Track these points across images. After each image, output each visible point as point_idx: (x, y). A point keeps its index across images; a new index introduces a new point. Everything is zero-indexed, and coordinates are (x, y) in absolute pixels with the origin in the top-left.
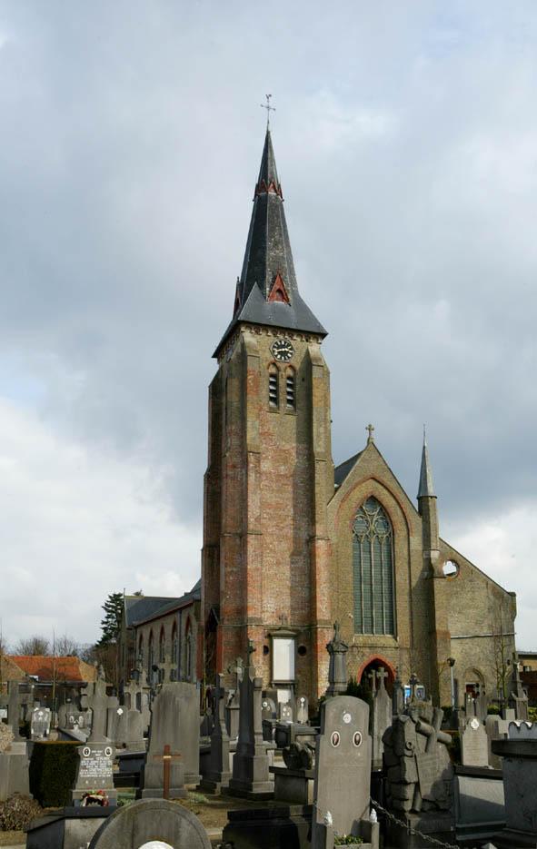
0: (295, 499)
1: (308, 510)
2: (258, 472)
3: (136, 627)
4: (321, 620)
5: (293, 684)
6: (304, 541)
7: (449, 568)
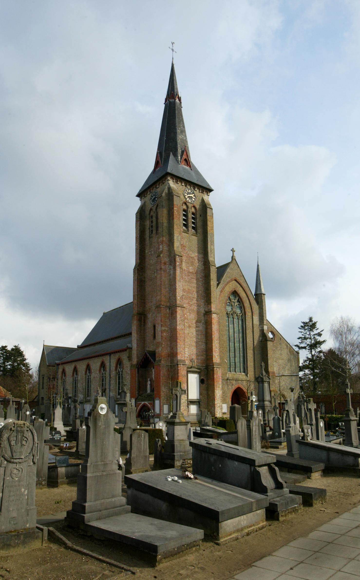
0: (197, 288)
1: (206, 296)
2: (181, 268)
3: (58, 365)
5: (199, 402)
6: (202, 314)
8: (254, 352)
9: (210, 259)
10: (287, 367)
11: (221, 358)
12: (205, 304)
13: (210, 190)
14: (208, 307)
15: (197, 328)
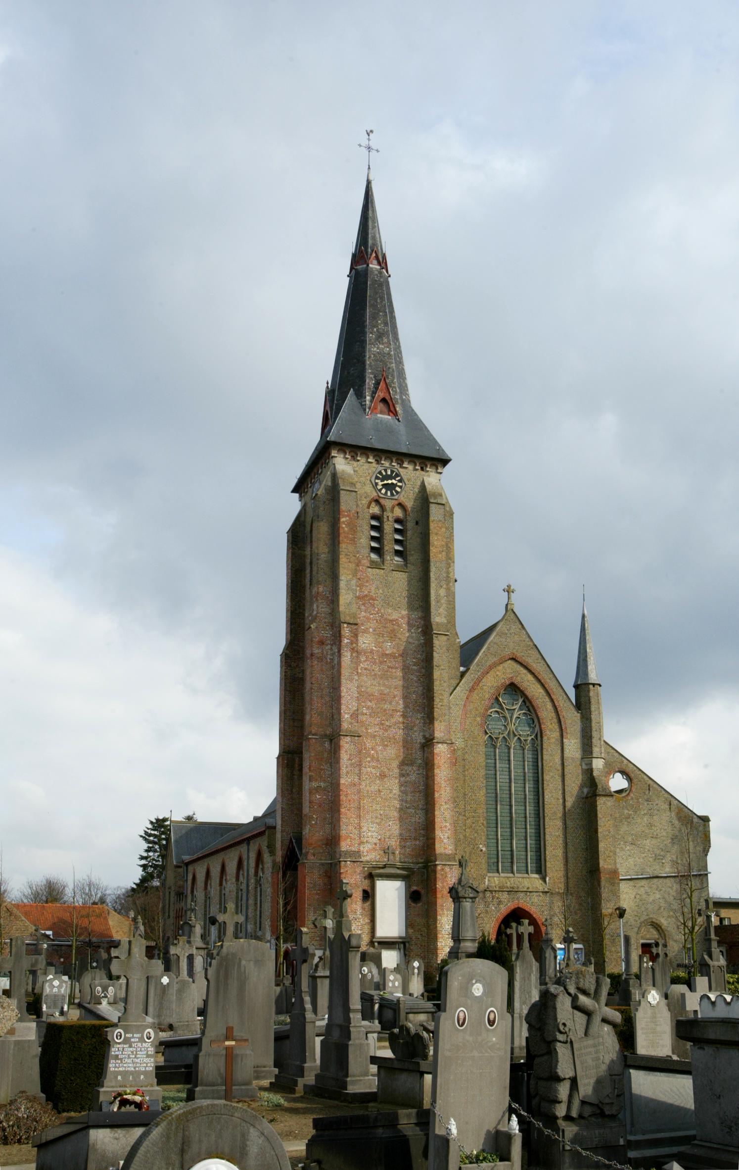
0: (406, 687)
1: (423, 703)
5: (404, 943)
7: (617, 782)
8: (565, 823)
10: (669, 857)
12: (424, 723)
14: (429, 729)
15: (403, 779)
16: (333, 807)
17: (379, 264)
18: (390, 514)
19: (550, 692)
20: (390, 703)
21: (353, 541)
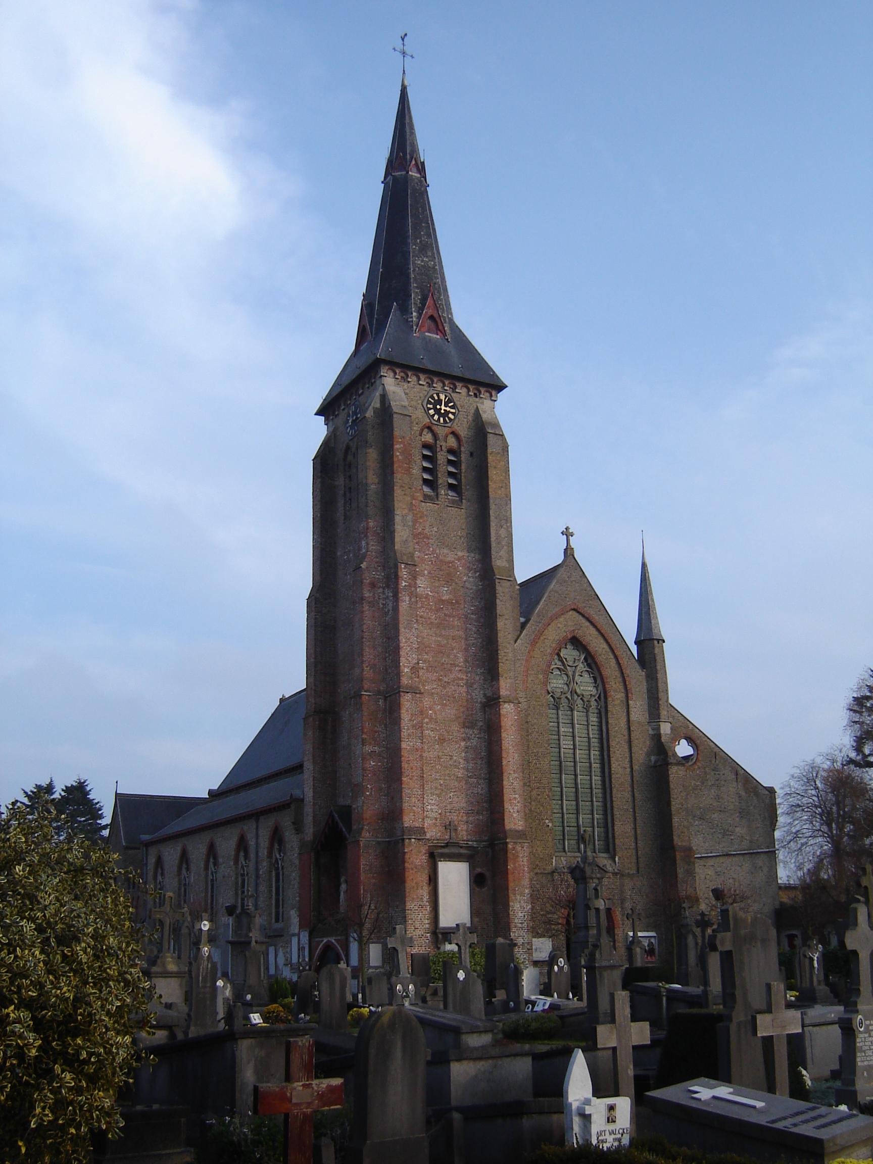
1: (488, 660)
4: (510, 830)
6: (478, 705)
7: (683, 749)
9: (498, 563)
11: (530, 815)
12: (484, 680)
13: (500, 387)
14: (492, 686)
16: (392, 774)
17: (419, 171)
18: (443, 444)
19: (614, 647)
20: (448, 656)
21: (408, 471)
